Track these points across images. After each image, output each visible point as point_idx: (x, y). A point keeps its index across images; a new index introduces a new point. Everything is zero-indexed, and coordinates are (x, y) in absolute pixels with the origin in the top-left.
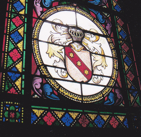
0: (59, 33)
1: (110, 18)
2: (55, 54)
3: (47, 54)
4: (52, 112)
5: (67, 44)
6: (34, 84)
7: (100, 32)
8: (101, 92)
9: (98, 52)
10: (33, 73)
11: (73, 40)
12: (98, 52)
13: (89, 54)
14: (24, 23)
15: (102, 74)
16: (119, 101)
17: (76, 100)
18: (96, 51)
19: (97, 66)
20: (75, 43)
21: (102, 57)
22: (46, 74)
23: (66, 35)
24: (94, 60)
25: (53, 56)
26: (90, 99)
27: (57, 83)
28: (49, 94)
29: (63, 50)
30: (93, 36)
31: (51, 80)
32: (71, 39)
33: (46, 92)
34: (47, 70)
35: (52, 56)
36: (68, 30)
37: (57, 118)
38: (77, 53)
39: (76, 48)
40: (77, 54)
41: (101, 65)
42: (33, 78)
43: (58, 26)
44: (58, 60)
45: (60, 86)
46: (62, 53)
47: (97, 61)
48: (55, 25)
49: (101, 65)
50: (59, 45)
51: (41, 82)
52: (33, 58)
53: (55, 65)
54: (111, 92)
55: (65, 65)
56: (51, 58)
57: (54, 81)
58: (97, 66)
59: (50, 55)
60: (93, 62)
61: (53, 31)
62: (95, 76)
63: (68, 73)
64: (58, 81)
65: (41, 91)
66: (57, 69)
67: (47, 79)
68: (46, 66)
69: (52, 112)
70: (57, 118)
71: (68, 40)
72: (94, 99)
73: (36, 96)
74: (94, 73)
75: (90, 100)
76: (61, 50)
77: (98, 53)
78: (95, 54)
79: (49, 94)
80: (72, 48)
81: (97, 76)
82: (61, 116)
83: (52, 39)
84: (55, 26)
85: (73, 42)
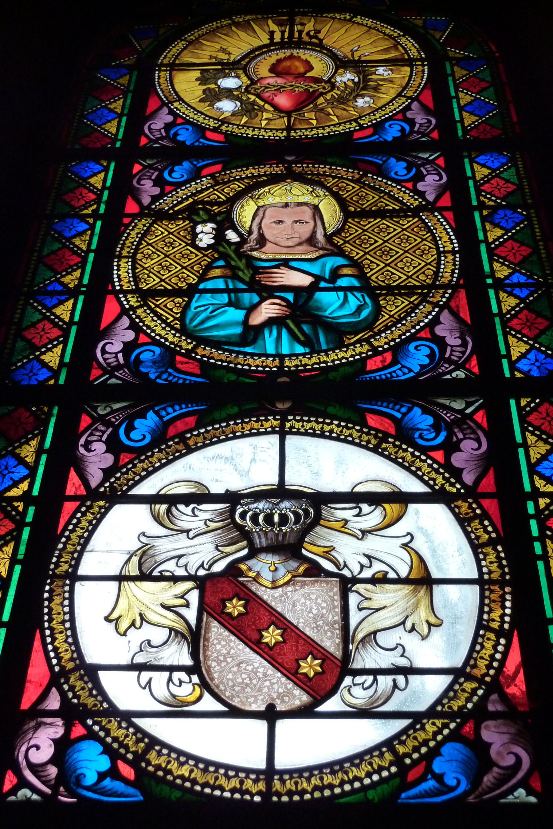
0: (182, 531)
1: (480, 417)
2: (151, 616)
3: (110, 621)
4: (61, 339)
5: (219, 567)
6: (24, 748)
7: (417, 487)
8: (389, 743)
9: (386, 568)
10: (26, 704)
11: (251, 545)
12: (386, 568)
13: (336, 589)
14: (20, 524)
15: (403, 662)
16: (501, 781)
17: (233, 791)
18: (378, 567)
19: (378, 634)
20: (263, 556)
21: (411, 587)
22: (90, 701)
23: (219, 531)
24: (360, 609)
25: (138, 623)
26: (314, 781)
27: (138, 729)
28: (91, 778)
29: (194, 597)
30: (365, 508)
31: (110, 722)
32: (245, 543)
33: (79, 772)
34: (97, 685)
35: (133, 624)
36: (232, 511)
37: (43, 350)
38: (266, 595)
39: (267, 576)
40: (265, 597)
41: (403, 623)
42: (23, 723)
43: (181, 507)
44: (162, 635)
45: (154, 742)
46: (187, 605)
47: (378, 610)
48: (164, 507)
49: (403, 623)
50: (175, 579)
51: (58, 736)
52: (41, 654)
53: (140, 659)
54: (454, 736)
55: (195, 654)
56: (125, 634)
57: (124, 725)
58: (375, 633)
59: (124, 625)
60: (354, 617)
61: (156, 529)
62: (359, 679)
63: (205, 685)
64: (141, 722)
65: (53, 771)
66: (146, 675)
67: (90, 722)
68: (288, 262)
69: (61, 339)
70: (43, 350)
71: (228, 549)
72: (337, 782)
73: (24, 793)
74: (357, 665)
75: (316, 788)
76: (182, 597)
77: (392, 575)
78: (373, 581)
79: (91, 778)
80: (241, 579)
81: (370, 678)
82: (21, 485)
83: (142, 561)
84: (169, 511)
85: (254, 553)
